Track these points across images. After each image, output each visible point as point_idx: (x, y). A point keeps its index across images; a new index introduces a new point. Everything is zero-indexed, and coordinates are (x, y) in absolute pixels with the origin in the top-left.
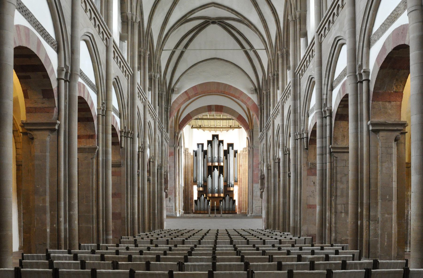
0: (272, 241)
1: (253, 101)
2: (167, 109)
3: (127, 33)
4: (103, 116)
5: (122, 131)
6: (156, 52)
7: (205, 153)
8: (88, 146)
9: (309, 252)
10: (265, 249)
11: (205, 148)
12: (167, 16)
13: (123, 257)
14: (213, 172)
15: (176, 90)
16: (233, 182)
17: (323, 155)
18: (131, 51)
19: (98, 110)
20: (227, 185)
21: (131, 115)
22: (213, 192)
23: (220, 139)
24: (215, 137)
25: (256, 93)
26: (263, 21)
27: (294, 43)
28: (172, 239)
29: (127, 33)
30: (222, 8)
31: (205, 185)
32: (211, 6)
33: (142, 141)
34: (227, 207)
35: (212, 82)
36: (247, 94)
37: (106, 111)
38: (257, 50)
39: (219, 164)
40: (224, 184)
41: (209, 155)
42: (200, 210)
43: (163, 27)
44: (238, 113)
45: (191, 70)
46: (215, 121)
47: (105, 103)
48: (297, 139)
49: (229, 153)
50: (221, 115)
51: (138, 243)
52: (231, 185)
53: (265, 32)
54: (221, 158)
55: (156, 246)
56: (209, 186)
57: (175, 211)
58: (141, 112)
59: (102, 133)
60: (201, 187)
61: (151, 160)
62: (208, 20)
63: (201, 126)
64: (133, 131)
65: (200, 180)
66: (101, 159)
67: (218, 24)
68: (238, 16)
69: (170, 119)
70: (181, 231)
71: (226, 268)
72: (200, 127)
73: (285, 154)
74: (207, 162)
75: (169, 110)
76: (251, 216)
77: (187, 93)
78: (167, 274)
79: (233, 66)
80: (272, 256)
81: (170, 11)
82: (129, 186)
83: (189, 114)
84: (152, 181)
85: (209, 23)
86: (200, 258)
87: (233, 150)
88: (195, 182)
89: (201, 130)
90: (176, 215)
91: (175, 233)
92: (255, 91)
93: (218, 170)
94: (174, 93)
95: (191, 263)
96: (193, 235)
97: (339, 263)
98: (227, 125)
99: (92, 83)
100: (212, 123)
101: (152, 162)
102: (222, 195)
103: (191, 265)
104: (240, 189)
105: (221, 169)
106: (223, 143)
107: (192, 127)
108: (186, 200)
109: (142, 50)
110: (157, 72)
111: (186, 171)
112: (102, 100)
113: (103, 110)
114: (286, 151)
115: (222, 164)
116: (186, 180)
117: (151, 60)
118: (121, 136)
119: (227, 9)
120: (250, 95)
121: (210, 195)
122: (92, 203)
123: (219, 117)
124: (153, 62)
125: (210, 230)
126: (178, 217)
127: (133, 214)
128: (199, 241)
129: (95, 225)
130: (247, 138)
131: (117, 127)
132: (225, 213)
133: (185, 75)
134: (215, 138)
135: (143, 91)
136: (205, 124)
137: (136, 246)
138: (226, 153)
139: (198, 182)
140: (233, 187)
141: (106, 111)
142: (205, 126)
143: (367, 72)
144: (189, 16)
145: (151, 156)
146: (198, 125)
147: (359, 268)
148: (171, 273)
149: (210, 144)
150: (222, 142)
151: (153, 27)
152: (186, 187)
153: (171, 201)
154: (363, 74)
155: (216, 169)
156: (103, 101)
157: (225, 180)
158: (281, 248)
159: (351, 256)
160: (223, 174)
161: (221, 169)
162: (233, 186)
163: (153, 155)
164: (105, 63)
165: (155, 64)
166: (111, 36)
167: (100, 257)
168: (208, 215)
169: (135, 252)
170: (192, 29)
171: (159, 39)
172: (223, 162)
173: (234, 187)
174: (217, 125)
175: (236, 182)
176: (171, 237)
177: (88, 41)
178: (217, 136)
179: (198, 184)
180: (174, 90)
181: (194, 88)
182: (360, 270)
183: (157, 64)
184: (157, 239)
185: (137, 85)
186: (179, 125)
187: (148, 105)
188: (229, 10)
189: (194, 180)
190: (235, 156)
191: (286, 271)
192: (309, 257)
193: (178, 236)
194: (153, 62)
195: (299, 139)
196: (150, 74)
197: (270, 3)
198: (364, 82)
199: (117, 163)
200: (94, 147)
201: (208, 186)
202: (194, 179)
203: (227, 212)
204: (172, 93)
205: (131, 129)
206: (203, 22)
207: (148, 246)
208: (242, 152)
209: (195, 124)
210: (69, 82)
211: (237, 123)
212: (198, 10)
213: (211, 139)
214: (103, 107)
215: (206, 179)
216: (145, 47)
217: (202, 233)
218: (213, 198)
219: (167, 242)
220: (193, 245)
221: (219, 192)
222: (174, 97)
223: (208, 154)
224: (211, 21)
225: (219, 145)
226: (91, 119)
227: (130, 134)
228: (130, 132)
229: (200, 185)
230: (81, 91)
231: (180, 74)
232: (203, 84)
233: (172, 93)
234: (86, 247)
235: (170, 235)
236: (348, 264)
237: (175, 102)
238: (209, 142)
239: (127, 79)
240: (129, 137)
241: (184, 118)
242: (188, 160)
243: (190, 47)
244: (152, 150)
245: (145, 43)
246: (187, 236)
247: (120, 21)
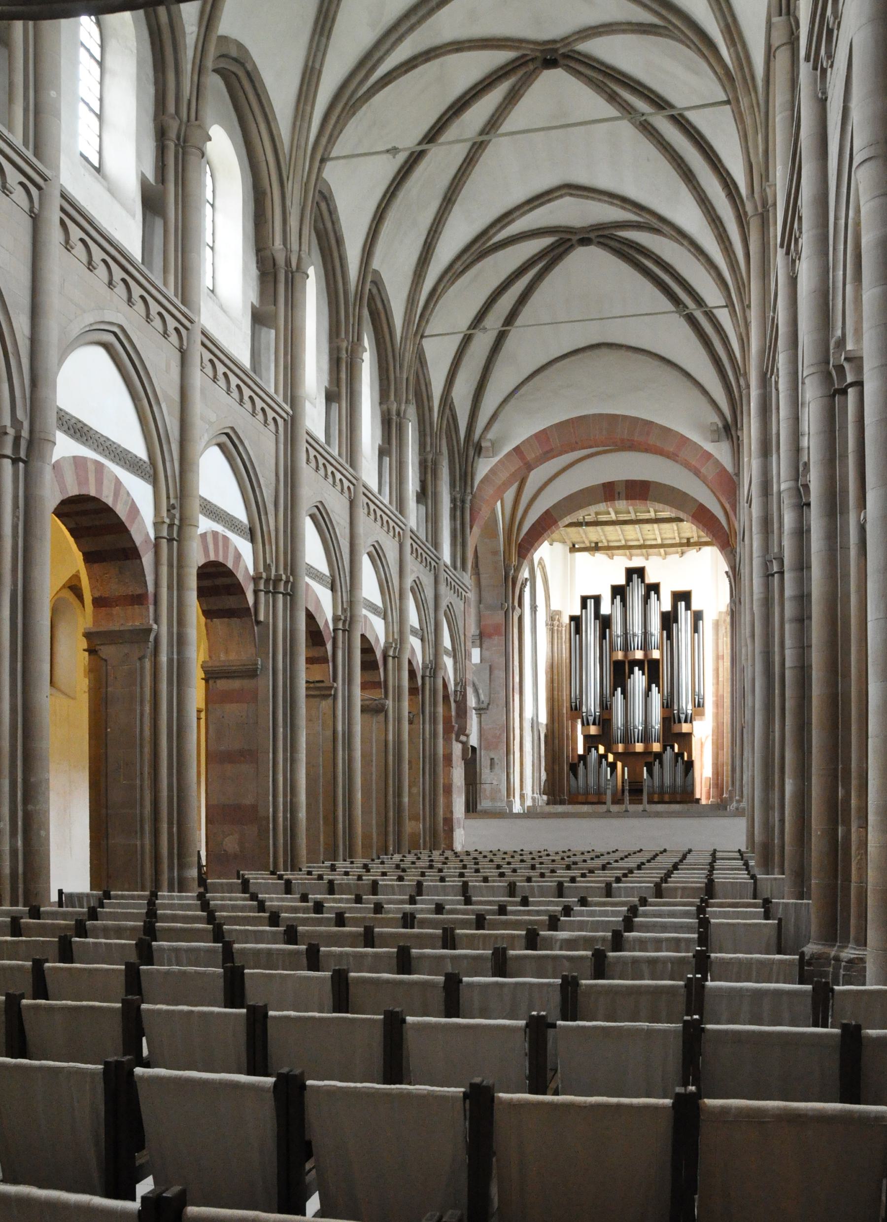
0: (633, 888)
1: (717, 462)
2: (463, 501)
3: (275, 303)
4: (170, 540)
5: (259, 576)
6: (401, 343)
7: (605, 623)
8: (130, 624)
9: (615, 921)
10: (345, 908)
11: (605, 609)
12: (429, 241)
13: (63, 924)
14: (629, 677)
15: (487, 448)
16: (690, 707)
17: (804, 620)
18: (286, 354)
19: (157, 525)
20: (671, 718)
21: (285, 532)
22: (627, 739)
23: (650, 579)
24: (635, 573)
25: (728, 439)
26: (713, 220)
27: (294, 325)
28: (573, 880)
29: (275, 305)
30: (593, 199)
31: (606, 717)
32: (561, 196)
33: (345, 600)
34: (667, 781)
35: (594, 415)
36: (700, 443)
37: (180, 528)
38: (715, 311)
39: (646, 655)
40: (663, 713)
41: (617, 628)
42: (587, 793)
43: (418, 272)
44: (696, 500)
45: (531, 383)
46: (637, 526)
47: (178, 506)
48: (773, 575)
49: (676, 621)
50: (652, 510)
51: (471, 892)
52: (683, 716)
53: (720, 254)
54: (651, 635)
55: (525, 902)
56: (618, 719)
57: (508, 795)
58: (337, 517)
59: (170, 588)
60: (594, 724)
61: (391, 653)
62: (568, 237)
63: (600, 545)
64: (291, 574)
65: (591, 704)
66: (164, 658)
67: (599, 243)
68: (639, 215)
69: (471, 528)
70: (602, 855)
71: (177, 956)
72: (595, 548)
74: (612, 649)
75: (468, 506)
76: (737, 809)
77: (522, 453)
78: (28, 969)
79: (656, 363)
80: (453, 930)
81: (435, 226)
82: (281, 730)
83: (547, 513)
84: (394, 712)
85: (569, 244)
86: (255, 932)
87: (689, 612)
88: (576, 709)
89: (600, 556)
90: (511, 810)
91: (585, 861)
92: (724, 434)
93: (643, 674)
94: (482, 455)
95: (169, 943)
96: (639, 867)
97: (581, 958)
98: (677, 538)
99: (129, 456)
100: (632, 533)
101: (394, 658)
102: (656, 747)
103: (169, 950)
104: (718, 728)
105: (653, 669)
106: (657, 592)
107: (573, 549)
108: (553, 762)
109: (344, 345)
110: (407, 401)
111: (556, 677)
112: (168, 498)
113: (171, 526)
115: (656, 654)
116: (556, 704)
117: (387, 370)
118: (256, 592)
119: (606, 198)
120: (709, 447)
121: (620, 748)
122: (142, 780)
123: (645, 516)
124: (395, 372)
125: (690, 851)
126: (518, 816)
127: (293, 808)
128: (658, 886)
129: (147, 842)
130: (727, 573)
131: (241, 565)
132: (661, 802)
133: (513, 402)
134: (635, 576)
136: (665, 536)
137: (468, 901)
138: (669, 620)
139: (584, 709)
140: (691, 722)
141: (180, 528)
142: (612, 544)
143: (855, 358)
145: (391, 641)
146: (591, 542)
147: (646, 973)
148: (38, 965)
149: (618, 597)
150: (655, 588)
152: (556, 725)
153: (497, 768)
154: (847, 366)
155: (636, 669)
156: (172, 501)
157: (665, 701)
158: (573, 909)
159: (693, 938)
160: (658, 685)
161: (653, 669)
162: (689, 720)
163: (396, 636)
164: (176, 396)
165: (401, 378)
167: (9, 924)
168: (602, 808)
169: (123, 913)
170: (521, 267)
171: (409, 307)
172: (660, 648)
173: (694, 723)
174: (648, 540)
175: (699, 706)
176: (571, 873)
177: (112, 345)
178: (640, 572)
179: (584, 714)
180: (481, 447)
181: (542, 436)
182: (653, 979)
183: (405, 377)
184: (529, 880)
186: (519, 544)
188: (615, 201)
189: (573, 704)
190: (696, 630)
191: (328, 974)
192: (561, 937)
193: (591, 871)
194: (395, 372)
195: (776, 573)
196: (385, 407)
197: (719, 166)
198: (850, 390)
199: (244, 665)
200: (145, 627)
201: (614, 720)
202: (573, 700)
203: (667, 798)
204: (476, 455)
205: (285, 569)
206: (552, 244)
207: (315, 898)
208: (723, 615)
209: (578, 540)
210: (24, 462)
211: (689, 529)
212: (521, 211)
213: (621, 581)
214: (172, 518)
215: (608, 699)
217: (666, 861)
218: (628, 756)
219: (560, 890)
220: (636, 900)
221: (646, 737)
222: (483, 467)
223: (614, 627)
224: (575, 238)
225: (646, 599)
226: (131, 553)
227: (282, 583)
228: (281, 580)
229: (591, 719)
230: (87, 479)
231: (500, 399)
232: (567, 421)
233: (476, 455)
234: (76, 899)
235: (568, 868)
236: (611, 960)
237: (486, 479)
238: (618, 591)
240: (261, 591)
241: (533, 525)
242: (562, 645)
243: (526, 315)
244: (393, 623)
245: (353, 325)
246: (619, 873)
247: (254, 271)
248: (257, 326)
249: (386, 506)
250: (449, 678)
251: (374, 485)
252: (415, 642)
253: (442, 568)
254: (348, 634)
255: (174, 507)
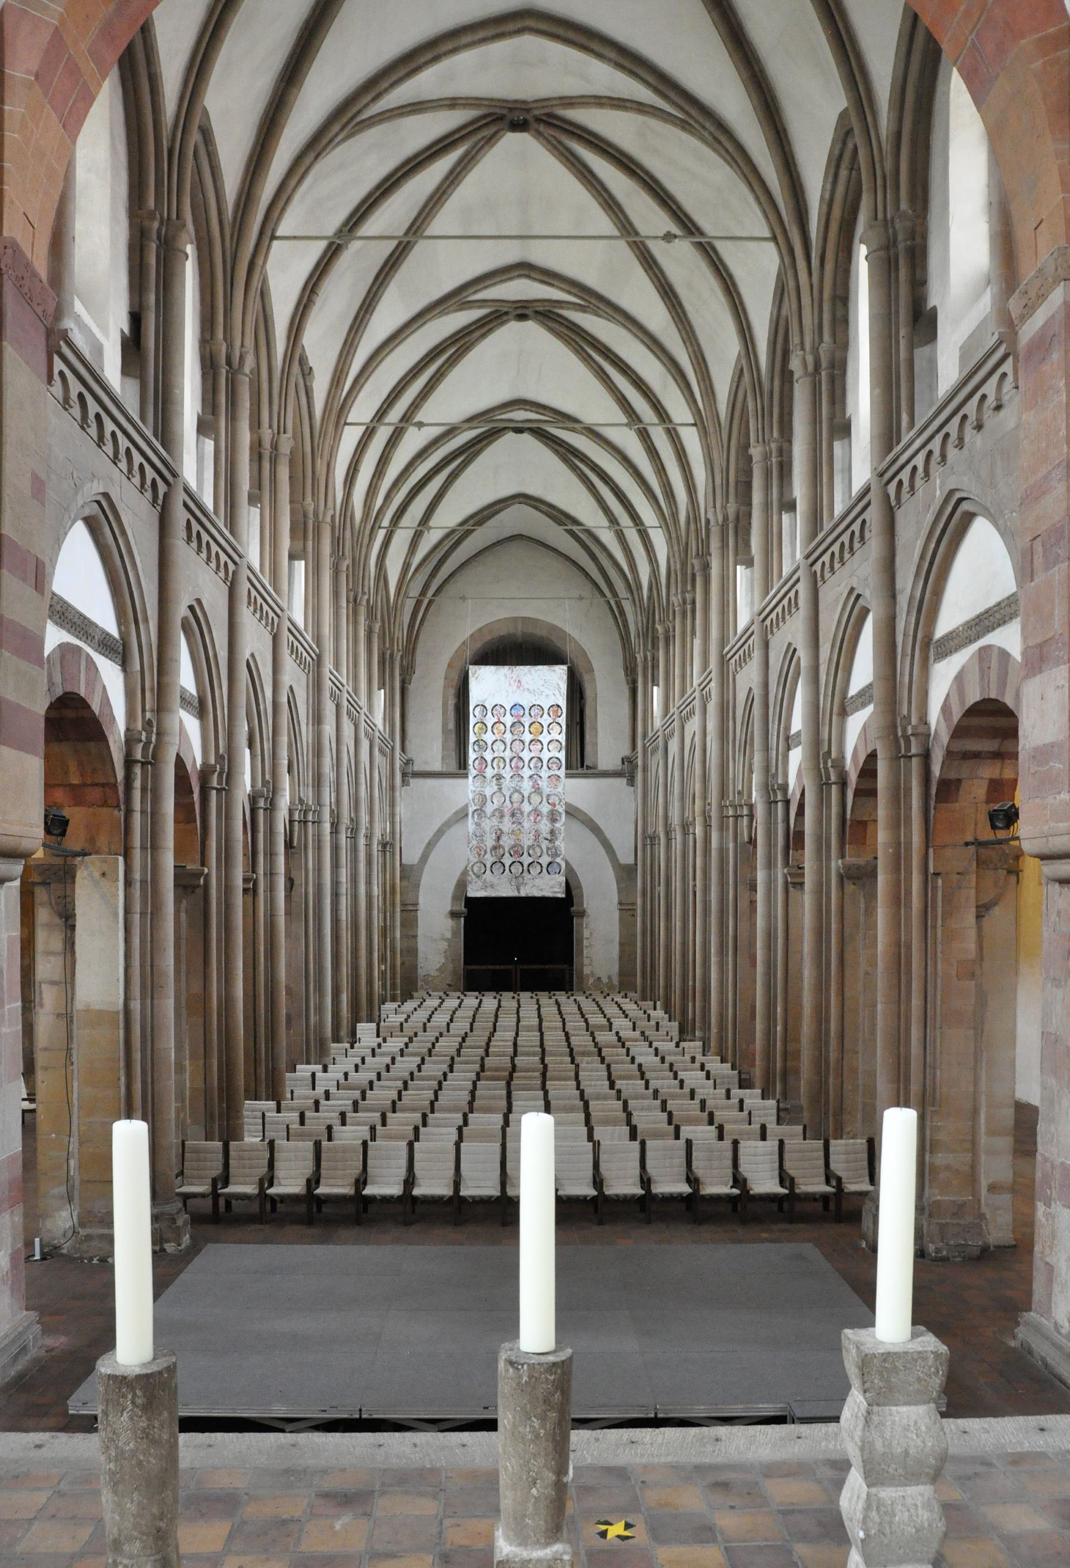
73: (770, 803)
114: (774, 791)
135: (227, 533)
144: (475, 292)
151: (310, 339)
166: (175, 475)
185: (289, 623)
187: (289, 630)
216: (169, 209)
239: (78, 417)
248: (201, 437)
249: (130, 420)
250: (106, 702)
251: (256, 565)
252: (191, 724)
253: (245, 573)
254: (226, 794)
255: (222, 757)
